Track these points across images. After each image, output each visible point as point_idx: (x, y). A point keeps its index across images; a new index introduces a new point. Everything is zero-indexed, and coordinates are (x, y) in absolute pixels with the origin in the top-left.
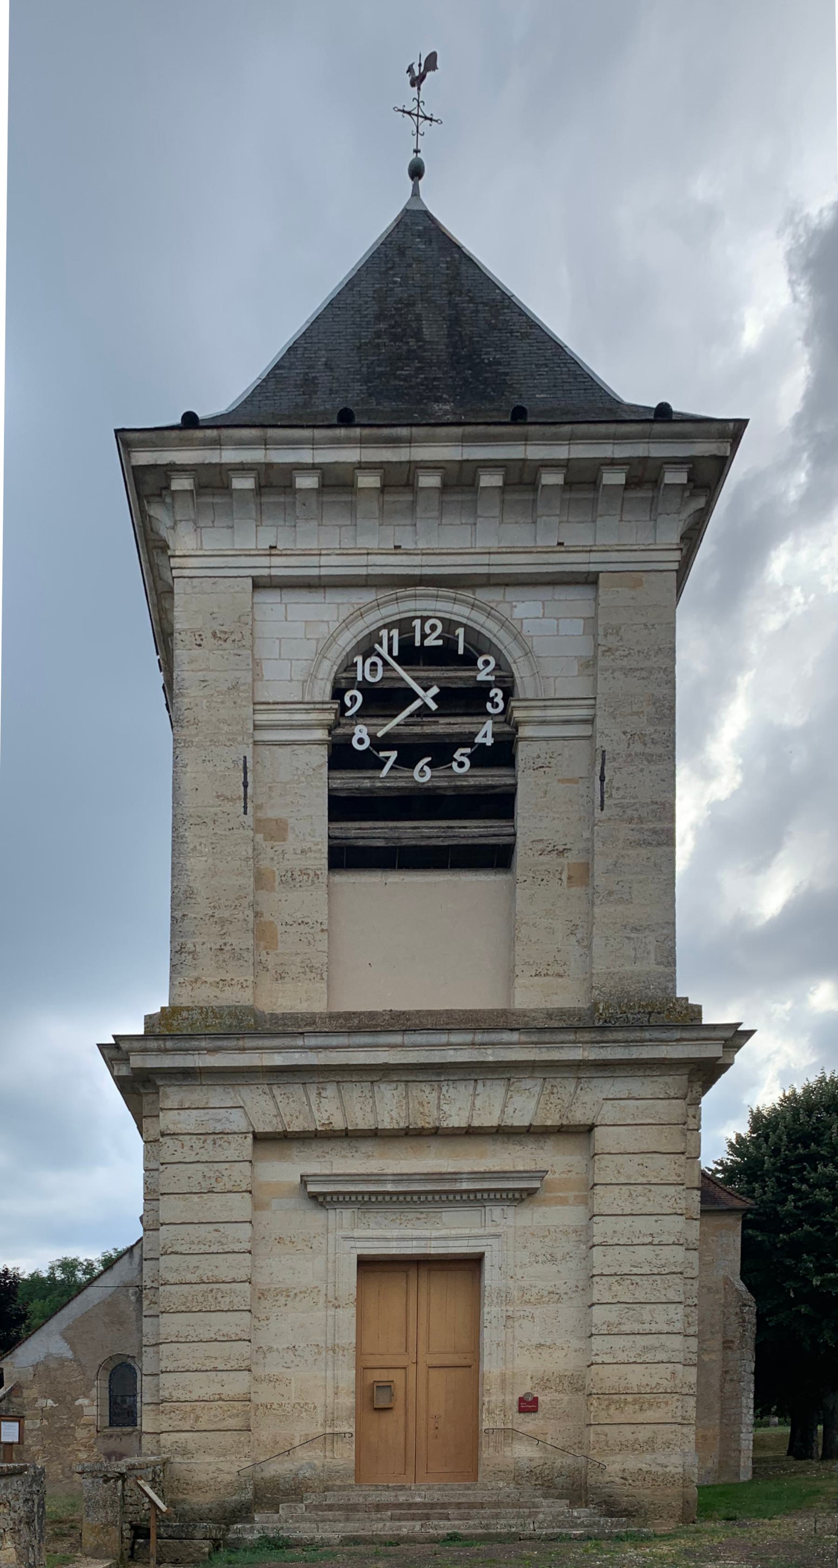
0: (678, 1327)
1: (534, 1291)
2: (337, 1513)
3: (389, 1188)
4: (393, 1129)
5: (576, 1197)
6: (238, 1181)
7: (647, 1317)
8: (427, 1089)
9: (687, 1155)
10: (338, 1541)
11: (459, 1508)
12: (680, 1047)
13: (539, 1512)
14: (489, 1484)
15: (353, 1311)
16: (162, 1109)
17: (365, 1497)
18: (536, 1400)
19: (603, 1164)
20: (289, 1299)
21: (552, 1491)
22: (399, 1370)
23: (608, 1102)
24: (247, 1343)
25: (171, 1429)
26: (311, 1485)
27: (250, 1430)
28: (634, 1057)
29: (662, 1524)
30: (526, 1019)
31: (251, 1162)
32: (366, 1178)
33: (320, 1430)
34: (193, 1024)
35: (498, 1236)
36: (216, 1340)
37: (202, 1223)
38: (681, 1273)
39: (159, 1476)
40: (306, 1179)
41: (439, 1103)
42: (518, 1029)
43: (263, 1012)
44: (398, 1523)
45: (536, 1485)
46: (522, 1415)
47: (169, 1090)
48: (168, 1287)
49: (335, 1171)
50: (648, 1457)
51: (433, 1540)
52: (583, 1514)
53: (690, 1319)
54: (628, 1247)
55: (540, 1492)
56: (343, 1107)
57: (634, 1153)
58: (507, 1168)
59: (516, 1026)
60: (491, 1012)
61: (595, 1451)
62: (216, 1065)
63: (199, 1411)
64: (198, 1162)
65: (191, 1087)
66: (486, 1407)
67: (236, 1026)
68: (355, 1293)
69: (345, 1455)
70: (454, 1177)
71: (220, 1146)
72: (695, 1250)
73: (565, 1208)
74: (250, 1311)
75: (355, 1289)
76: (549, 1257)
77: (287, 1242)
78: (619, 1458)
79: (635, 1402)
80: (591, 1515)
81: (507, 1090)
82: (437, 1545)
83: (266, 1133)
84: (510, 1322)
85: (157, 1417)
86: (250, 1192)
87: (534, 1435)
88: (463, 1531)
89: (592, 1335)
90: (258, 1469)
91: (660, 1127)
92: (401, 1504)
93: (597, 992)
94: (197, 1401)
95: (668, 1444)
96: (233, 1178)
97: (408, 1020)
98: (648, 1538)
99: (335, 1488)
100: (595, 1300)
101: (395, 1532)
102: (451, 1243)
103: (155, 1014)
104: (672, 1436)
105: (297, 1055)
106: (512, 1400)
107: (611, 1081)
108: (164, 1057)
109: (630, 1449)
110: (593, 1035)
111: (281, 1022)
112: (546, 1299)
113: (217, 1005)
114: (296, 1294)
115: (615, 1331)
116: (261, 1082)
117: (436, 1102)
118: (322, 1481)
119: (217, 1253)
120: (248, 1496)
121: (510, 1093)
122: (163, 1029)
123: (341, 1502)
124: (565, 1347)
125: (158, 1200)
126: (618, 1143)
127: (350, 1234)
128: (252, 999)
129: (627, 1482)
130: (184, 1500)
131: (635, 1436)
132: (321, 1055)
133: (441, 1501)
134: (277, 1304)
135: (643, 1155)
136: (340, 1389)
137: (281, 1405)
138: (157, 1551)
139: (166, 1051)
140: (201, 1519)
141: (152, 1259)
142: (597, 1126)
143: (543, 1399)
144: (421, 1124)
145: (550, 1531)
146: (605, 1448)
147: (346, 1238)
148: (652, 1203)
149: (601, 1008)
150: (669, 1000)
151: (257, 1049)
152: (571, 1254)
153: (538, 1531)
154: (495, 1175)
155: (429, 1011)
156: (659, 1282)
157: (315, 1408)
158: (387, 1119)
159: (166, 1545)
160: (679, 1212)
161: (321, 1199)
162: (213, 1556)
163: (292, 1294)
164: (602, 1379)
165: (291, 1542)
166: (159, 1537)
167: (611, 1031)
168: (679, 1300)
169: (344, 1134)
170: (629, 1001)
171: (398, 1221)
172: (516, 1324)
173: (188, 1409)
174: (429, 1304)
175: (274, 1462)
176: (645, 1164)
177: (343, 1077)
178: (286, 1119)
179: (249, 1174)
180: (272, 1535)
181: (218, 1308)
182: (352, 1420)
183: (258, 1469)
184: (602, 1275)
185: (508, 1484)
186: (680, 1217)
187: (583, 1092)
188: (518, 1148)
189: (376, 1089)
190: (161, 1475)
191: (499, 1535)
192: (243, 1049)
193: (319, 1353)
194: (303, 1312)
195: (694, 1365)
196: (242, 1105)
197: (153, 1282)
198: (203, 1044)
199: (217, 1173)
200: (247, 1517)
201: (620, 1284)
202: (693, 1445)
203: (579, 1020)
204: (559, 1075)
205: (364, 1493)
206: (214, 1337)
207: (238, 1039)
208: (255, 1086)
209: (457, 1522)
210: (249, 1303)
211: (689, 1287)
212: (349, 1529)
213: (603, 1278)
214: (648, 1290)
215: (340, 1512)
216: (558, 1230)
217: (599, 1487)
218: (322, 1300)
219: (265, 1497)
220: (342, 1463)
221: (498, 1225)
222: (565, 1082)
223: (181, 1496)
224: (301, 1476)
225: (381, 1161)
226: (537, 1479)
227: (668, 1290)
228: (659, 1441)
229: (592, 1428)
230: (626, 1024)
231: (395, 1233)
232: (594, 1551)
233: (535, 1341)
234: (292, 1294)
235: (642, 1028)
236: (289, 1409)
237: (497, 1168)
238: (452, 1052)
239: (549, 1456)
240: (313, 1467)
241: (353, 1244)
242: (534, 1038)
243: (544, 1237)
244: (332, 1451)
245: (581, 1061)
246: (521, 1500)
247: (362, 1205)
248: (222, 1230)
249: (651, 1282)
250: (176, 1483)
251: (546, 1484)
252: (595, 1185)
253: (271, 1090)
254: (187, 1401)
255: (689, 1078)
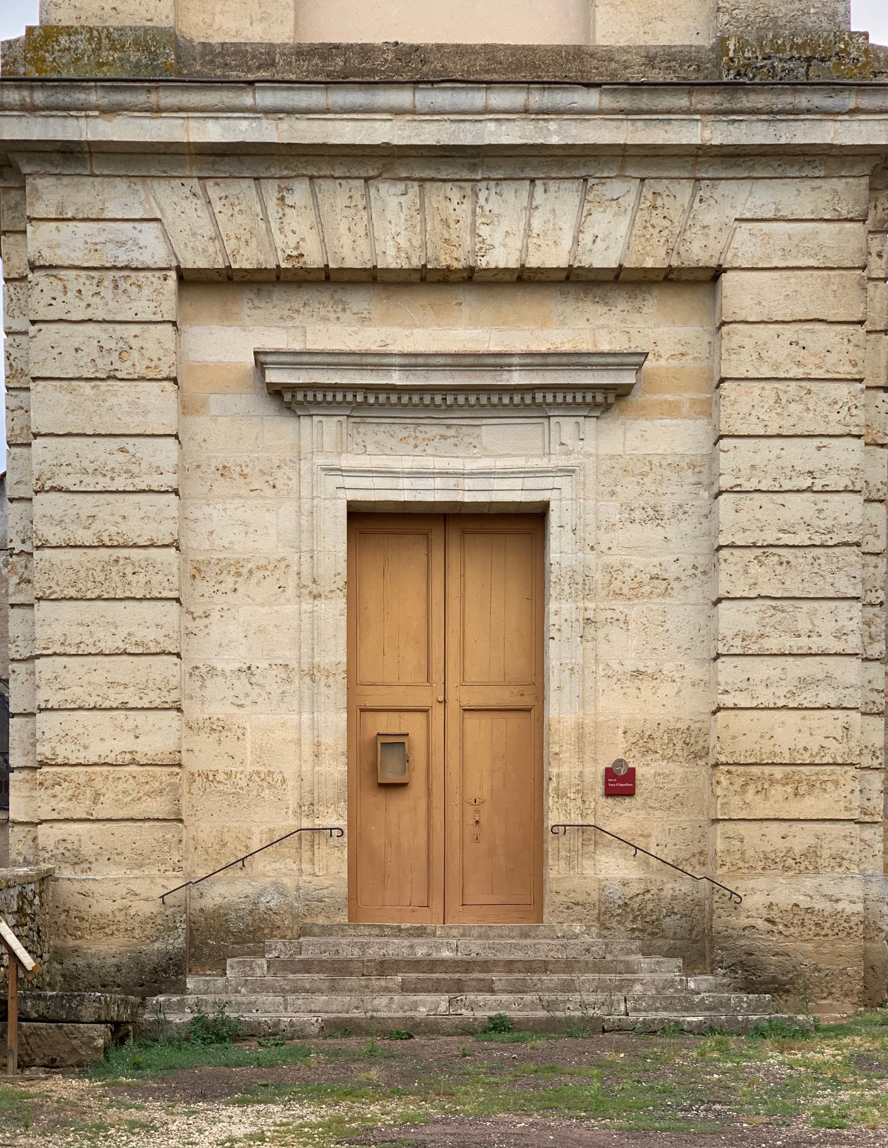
0: (853, 643)
1: (629, 573)
2: (316, 976)
3: (396, 379)
4: (401, 269)
5: (693, 402)
6: (155, 358)
7: (804, 625)
8: (456, 195)
9: (868, 326)
10: (315, 1029)
11: (511, 971)
12: (855, 125)
13: (634, 981)
14: (558, 927)
15: (341, 603)
16: (31, 219)
17: (363, 947)
18: (632, 772)
19: (736, 341)
20: (240, 579)
21: (659, 942)
22: (418, 714)
23: (745, 225)
24: (175, 659)
25: (55, 816)
26: (279, 923)
27: (181, 821)
28: (783, 141)
29: (831, 1008)
30: (613, 65)
31: (174, 323)
32: (357, 360)
33: (292, 823)
34: (78, 59)
35: (569, 472)
36: (125, 653)
37: (100, 435)
38: (858, 545)
39: (31, 903)
40: (263, 358)
41: (474, 223)
42: (598, 85)
43: (191, 41)
44: (412, 998)
45: (633, 930)
46: (610, 801)
47: (42, 183)
48: (47, 551)
49: (311, 346)
50: (809, 883)
51: (467, 1030)
52: (704, 986)
53: (873, 629)
54: (774, 496)
55: (638, 943)
56: (320, 226)
57: (783, 322)
58: (584, 347)
59: (597, 79)
60: (557, 50)
61: (725, 869)
62: (115, 139)
63: (98, 783)
64: (90, 320)
65: (76, 179)
66: (553, 785)
67: (146, 66)
68: (345, 573)
69: (333, 869)
70: (499, 361)
71: (125, 291)
72: (881, 501)
73: (675, 422)
74: (178, 600)
75: (345, 565)
76: (651, 513)
77: (236, 476)
78: (762, 883)
79: (786, 780)
80: (718, 988)
81: (583, 200)
82: (471, 1039)
83: (199, 270)
84: (590, 631)
85: (34, 793)
86: (175, 380)
87: (628, 839)
88: (515, 1014)
89: (718, 656)
90: (195, 892)
91: (825, 273)
92: (419, 961)
93: (726, 18)
94: (95, 764)
95: (839, 859)
96: (147, 354)
97: (424, 62)
98: (804, 1033)
99: (316, 930)
100: (722, 593)
101: (409, 1014)
102: (497, 484)
103: (17, 40)
104: (845, 845)
105: (244, 124)
106: (594, 774)
107: (747, 184)
108: (32, 120)
109: (780, 866)
110: (718, 99)
111: (219, 60)
112: (646, 589)
113: (116, 24)
114: (250, 572)
115: (755, 649)
116: (188, 173)
117: (469, 220)
118: (295, 917)
119: (124, 492)
120: (177, 942)
121: (587, 206)
122: (29, 67)
123: (325, 957)
124: (677, 676)
125: (28, 389)
126: (760, 303)
127: (334, 462)
128: (172, 16)
129: (774, 928)
130: (76, 950)
131: (787, 843)
132: (284, 125)
133: (483, 957)
134: (222, 588)
135: (798, 326)
136: (323, 747)
137: (229, 775)
138: (21, 1044)
139: (32, 109)
140: (104, 986)
141: (21, 499)
142: (725, 271)
143: (644, 771)
144: (445, 261)
145: (651, 1015)
146: (741, 864)
147: (330, 470)
148: (811, 415)
149: (732, 47)
150: (839, 38)
151: (181, 110)
152: (686, 508)
153: (633, 1016)
154: (564, 360)
155: (458, 46)
156: (822, 561)
157: (284, 781)
158: (392, 252)
159: (35, 1033)
160: (855, 432)
161: (288, 397)
162: (112, 1055)
163: (245, 571)
164: (734, 738)
165: (243, 1030)
166: (23, 1017)
167: (747, 92)
168: (854, 595)
169: (323, 276)
170: (775, 37)
171: (412, 441)
172: (601, 634)
173: (82, 780)
174: (463, 596)
175: (220, 879)
176: (802, 343)
177: (320, 169)
178: (230, 246)
179: (173, 348)
180: (211, 1016)
181: (128, 594)
182: (343, 805)
183: (195, 892)
184: (733, 546)
185: (588, 927)
186: (856, 440)
187: (704, 205)
188: (601, 309)
189: (373, 191)
190: (37, 901)
191: (569, 1020)
192: (156, 110)
193: (289, 681)
194: (262, 605)
195: (879, 714)
196: (159, 217)
197: (23, 542)
198: (94, 98)
199: (121, 344)
200: (176, 982)
201: (761, 564)
202: (880, 862)
203: (698, 69)
204: (666, 174)
205: (361, 940)
206: (122, 646)
207: (149, 90)
208: (178, 182)
209: (504, 997)
210: (176, 586)
211: (871, 569)
212: (335, 1007)
213: (736, 551)
214: (806, 575)
215: (322, 976)
216: (664, 463)
217: (731, 937)
218: (291, 583)
219: (207, 944)
220: (327, 883)
221: (569, 453)
222: (675, 187)
223: (71, 942)
224: (262, 908)
225: (383, 330)
226: (635, 919)
227: (837, 576)
228: (826, 853)
229: (719, 826)
230: (770, 80)
231: (407, 463)
232: (715, 1055)
233: (631, 665)
234: (245, 571)
235: (796, 86)
236: (243, 783)
237: (567, 348)
238: (492, 126)
239: (654, 877)
240: (282, 892)
241: (339, 480)
242: (624, 102)
243: (643, 475)
244: (312, 861)
245: (699, 147)
246: (609, 958)
247: (353, 409)
248: (132, 450)
249: (811, 561)
250: (63, 917)
251: (650, 929)
252: (723, 380)
253: (205, 190)
254: (80, 764)
255: (871, 183)
